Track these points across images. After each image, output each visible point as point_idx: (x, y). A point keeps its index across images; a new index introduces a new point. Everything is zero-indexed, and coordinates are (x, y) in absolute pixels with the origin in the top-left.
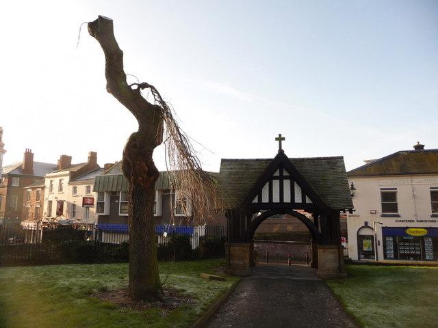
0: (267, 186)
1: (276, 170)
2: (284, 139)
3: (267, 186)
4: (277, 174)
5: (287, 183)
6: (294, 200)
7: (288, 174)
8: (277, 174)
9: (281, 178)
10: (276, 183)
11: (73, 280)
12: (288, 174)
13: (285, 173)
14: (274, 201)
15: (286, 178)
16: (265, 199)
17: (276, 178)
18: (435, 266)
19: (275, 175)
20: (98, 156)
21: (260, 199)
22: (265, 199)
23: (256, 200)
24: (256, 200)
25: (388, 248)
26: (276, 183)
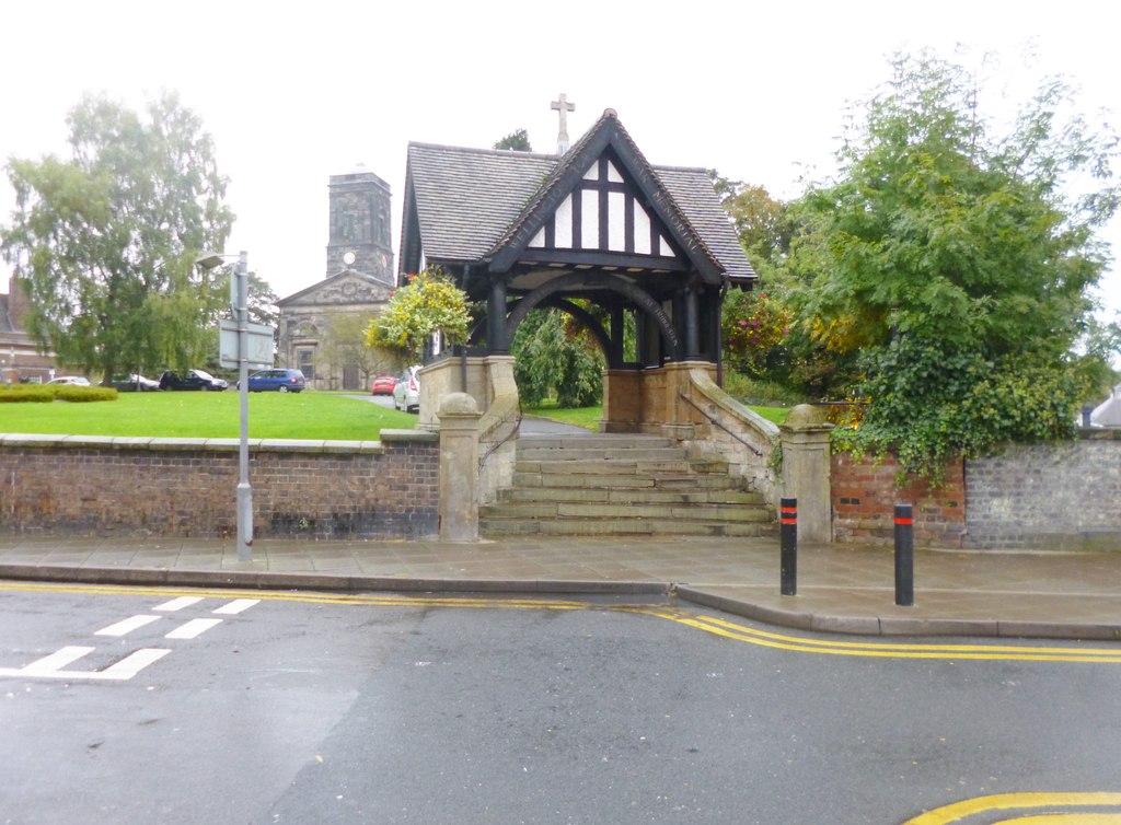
0: (567, 205)
1: (607, 164)
2: (571, 108)
3: (567, 205)
4: (593, 174)
5: (617, 200)
6: (553, 243)
7: (621, 180)
8: (593, 174)
9: (604, 187)
10: (590, 198)
11: (945, 525)
12: (621, 180)
13: (614, 176)
14: (612, 247)
15: (616, 187)
16: (563, 240)
17: (591, 185)
18: (1119, 656)
19: (586, 177)
20: (623, 119)
21: (550, 236)
22: (563, 240)
23: (539, 241)
24: (539, 241)
25: (584, 498)
26: (590, 198)
